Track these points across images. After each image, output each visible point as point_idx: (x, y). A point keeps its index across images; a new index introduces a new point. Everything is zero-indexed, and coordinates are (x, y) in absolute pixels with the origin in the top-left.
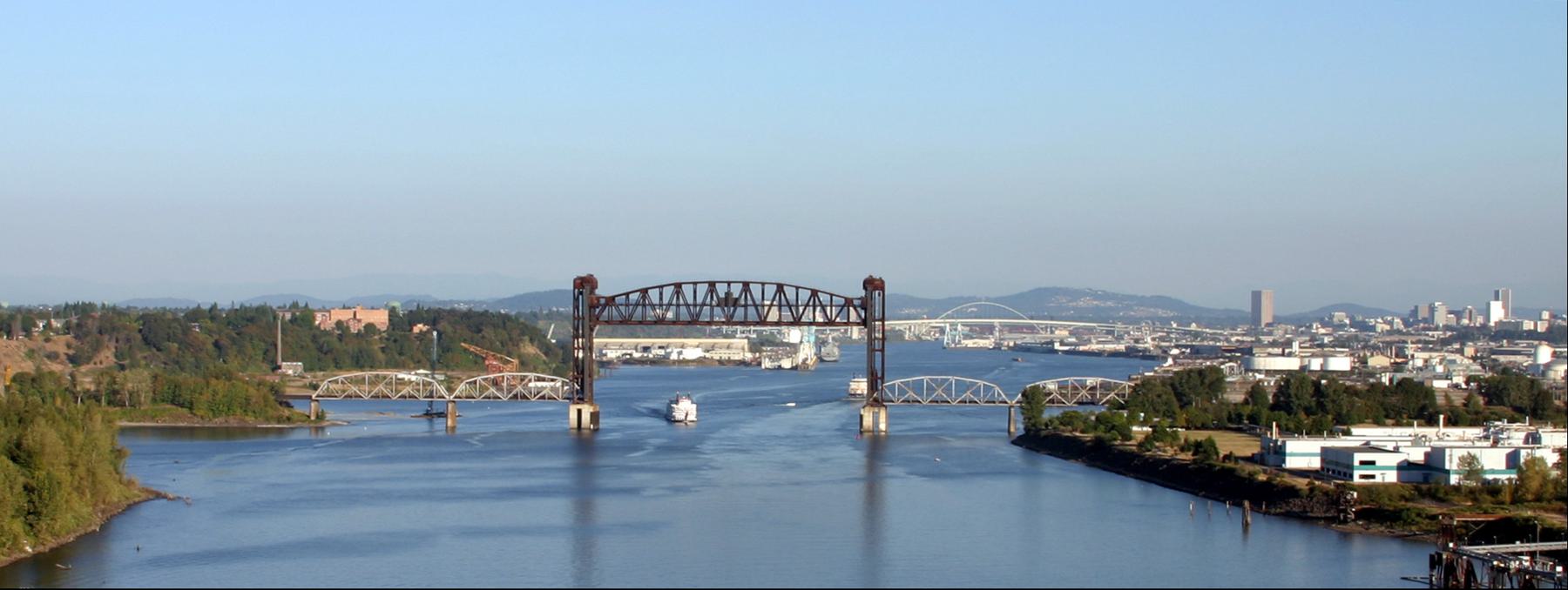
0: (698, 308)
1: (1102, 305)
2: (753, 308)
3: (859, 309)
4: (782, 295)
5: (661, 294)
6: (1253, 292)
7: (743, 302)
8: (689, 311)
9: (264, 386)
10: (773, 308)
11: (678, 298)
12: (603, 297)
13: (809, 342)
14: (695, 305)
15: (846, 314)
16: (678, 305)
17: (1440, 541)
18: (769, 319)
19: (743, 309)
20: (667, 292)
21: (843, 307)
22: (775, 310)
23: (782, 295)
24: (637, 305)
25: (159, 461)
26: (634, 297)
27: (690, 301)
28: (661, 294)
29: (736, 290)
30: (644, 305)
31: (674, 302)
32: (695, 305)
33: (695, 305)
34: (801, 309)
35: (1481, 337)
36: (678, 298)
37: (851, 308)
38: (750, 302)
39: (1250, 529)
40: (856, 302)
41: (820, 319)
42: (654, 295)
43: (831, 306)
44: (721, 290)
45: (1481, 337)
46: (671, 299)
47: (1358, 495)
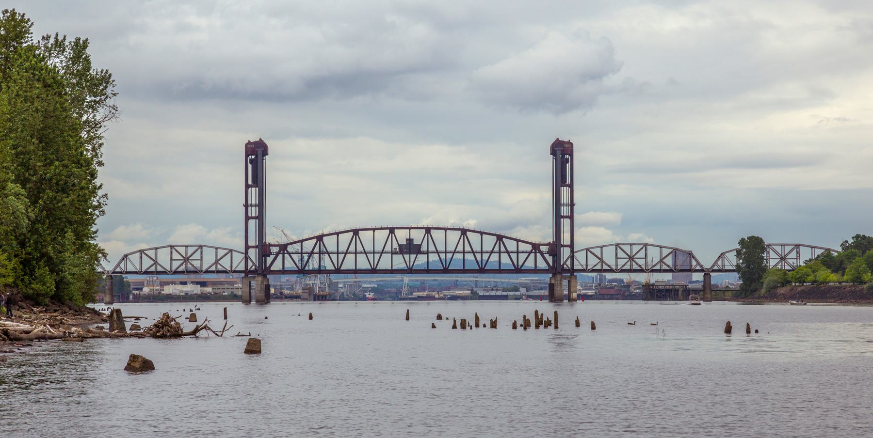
2: (509, 249)
3: (547, 256)
4: (321, 243)
6: (153, 369)
9: (268, 287)
13: (6, 272)
16: (500, 252)
18: (380, 267)
19: (534, 254)
20: (346, 238)
21: (530, 253)
23: (321, 243)
24: (311, 253)
25: (305, 302)
26: (308, 246)
29: (418, 237)
37: (538, 255)
38: (468, 248)
39: (723, 428)
40: (544, 249)
41: (329, 267)
42: (330, 243)
43: (518, 252)
44: (402, 236)
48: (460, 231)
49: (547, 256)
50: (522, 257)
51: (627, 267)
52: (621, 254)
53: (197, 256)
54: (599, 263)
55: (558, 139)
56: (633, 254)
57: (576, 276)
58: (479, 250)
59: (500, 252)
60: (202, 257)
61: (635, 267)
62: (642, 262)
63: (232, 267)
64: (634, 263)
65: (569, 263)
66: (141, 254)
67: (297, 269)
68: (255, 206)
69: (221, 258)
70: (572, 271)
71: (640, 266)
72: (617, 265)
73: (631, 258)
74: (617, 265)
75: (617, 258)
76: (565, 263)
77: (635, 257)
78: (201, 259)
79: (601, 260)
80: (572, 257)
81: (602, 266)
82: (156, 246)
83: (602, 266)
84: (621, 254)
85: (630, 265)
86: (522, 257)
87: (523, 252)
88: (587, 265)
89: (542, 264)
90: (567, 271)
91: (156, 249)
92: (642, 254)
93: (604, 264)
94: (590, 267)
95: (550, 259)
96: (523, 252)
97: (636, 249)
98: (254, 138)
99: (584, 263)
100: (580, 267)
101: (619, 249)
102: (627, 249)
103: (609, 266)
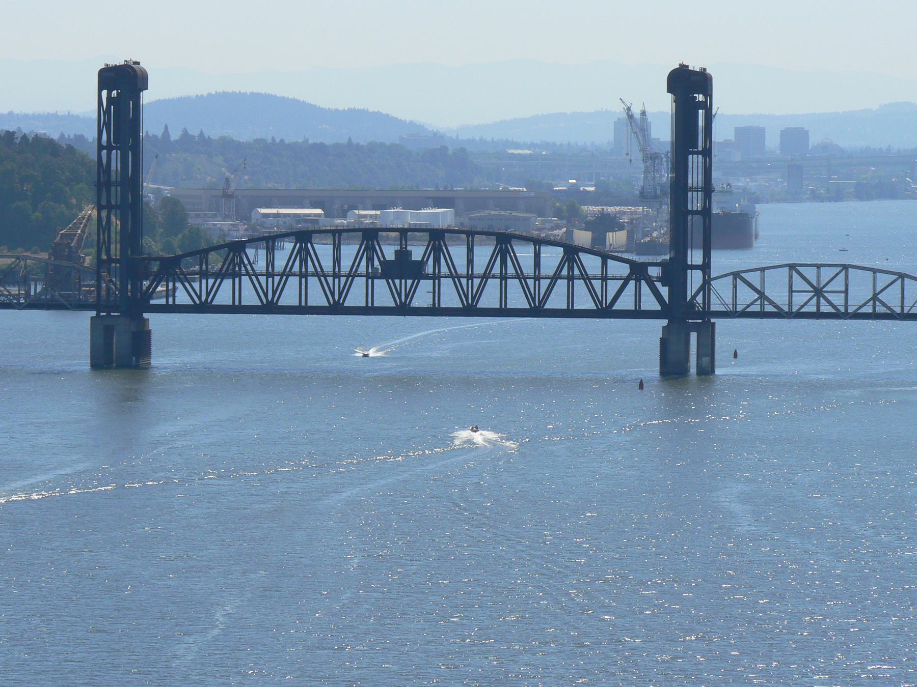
0: (477, 281)
1: (517, 152)
2: (591, 272)
3: (658, 285)
5: (537, 256)
7: (429, 269)
8: (525, 288)
10: (551, 272)
11: (504, 263)
12: (156, 259)
14: (470, 277)
15: (906, 301)
17: (491, 188)
18: (617, 307)
20: (287, 248)
22: (493, 285)
24: (286, 274)
27: (462, 269)
28: (537, 256)
30: (303, 275)
31: (496, 270)
32: (470, 277)
33: (336, 275)
34: (545, 284)
35: (77, 246)
36: (504, 263)
38: (511, 271)
40: (654, 272)
45: (77, 246)
46: (560, 268)
47: (526, 189)
48: (361, 233)
49: (658, 285)
50: (613, 287)
51: (812, 308)
52: (798, 283)
53: (838, 284)
54: (756, 300)
55: (705, 69)
56: (821, 286)
57: (714, 324)
58: (598, 272)
59: (504, 278)
60: (847, 286)
61: (825, 308)
62: (838, 300)
63: (902, 308)
64: (822, 301)
65: (699, 299)
66: (735, 279)
67: (193, 304)
68: (692, 189)
69: (735, 287)
70: (707, 314)
71: (834, 306)
72: (790, 304)
73: (818, 292)
74: (790, 304)
75: (791, 291)
76: (694, 297)
77: (824, 289)
78: (846, 292)
79: (762, 295)
80: (706, 287)
81: (762, 305)
82: (877, 265)
83: (762, 305)
84: (798, 283)
85: (761, 305)
86: (613, 287)
87: (614, 278)
88: (735, 304)
89: (650, 303)
90: (698, 315)
91: (762, 270)
92: (838, 284)
93: (766, 302)
94: (851, 310)
95: (664, 291)
96: (614, 278)
97: (826, 274)
98: (695, 65)
99: (729, 299)
100: (722, 308)
101: (795, 274)
102: (811, 274)
103: (776, 306)
